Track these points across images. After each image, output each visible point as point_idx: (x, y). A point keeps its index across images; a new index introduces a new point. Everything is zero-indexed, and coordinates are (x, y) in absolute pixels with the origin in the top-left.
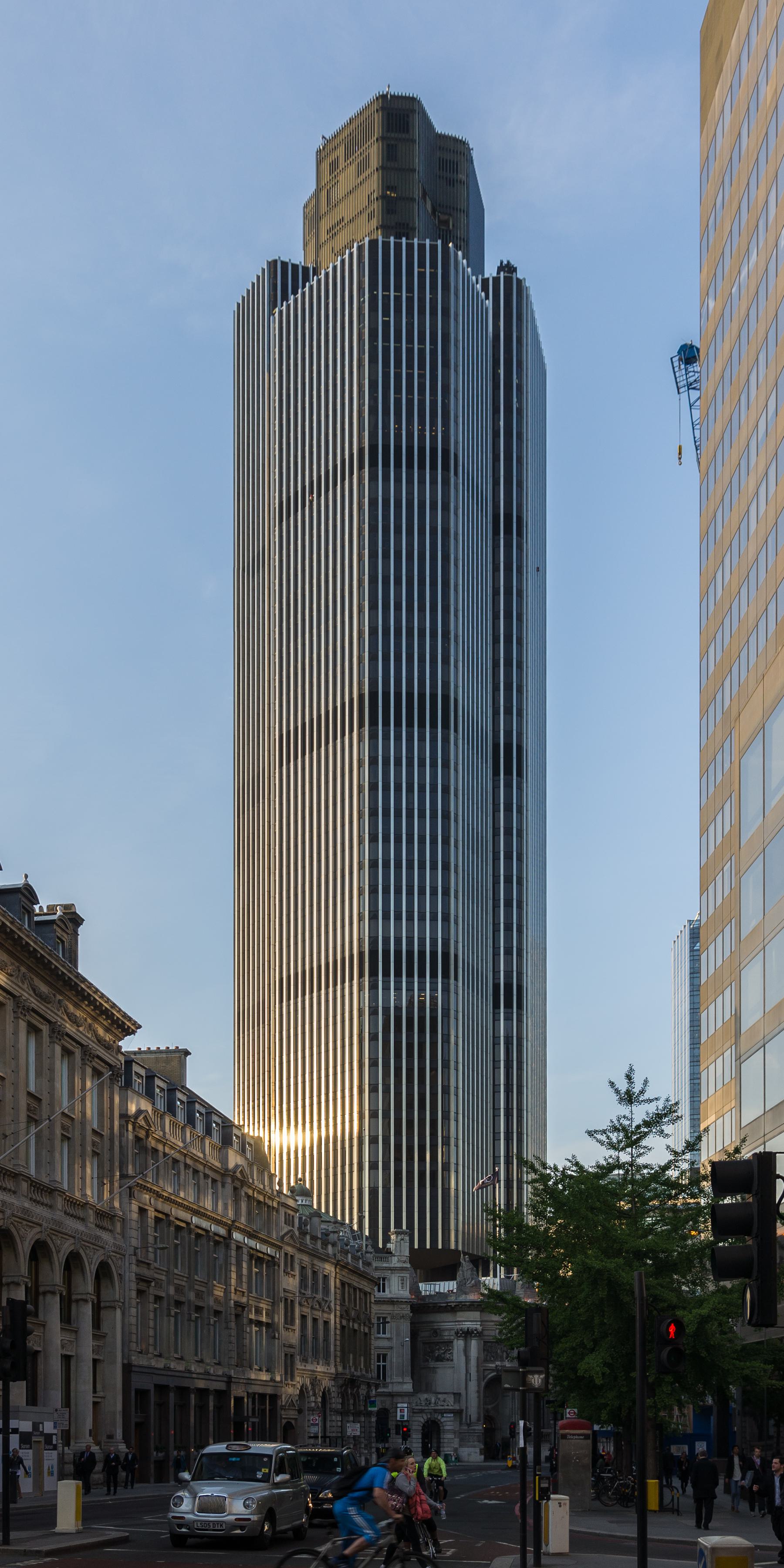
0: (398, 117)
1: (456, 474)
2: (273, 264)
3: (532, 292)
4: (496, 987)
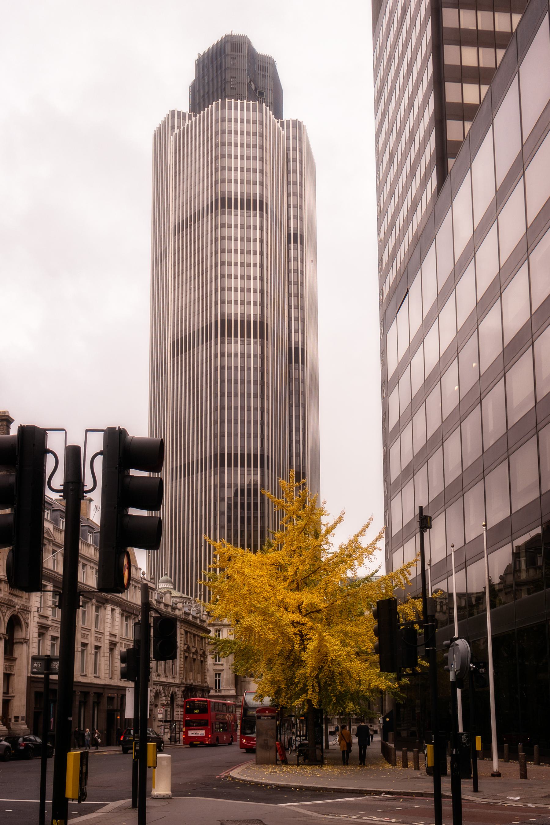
0: (233, 74)
1: (267, 213)
2: (173, 112)
3: (307, 128)
4: (290, 349)
